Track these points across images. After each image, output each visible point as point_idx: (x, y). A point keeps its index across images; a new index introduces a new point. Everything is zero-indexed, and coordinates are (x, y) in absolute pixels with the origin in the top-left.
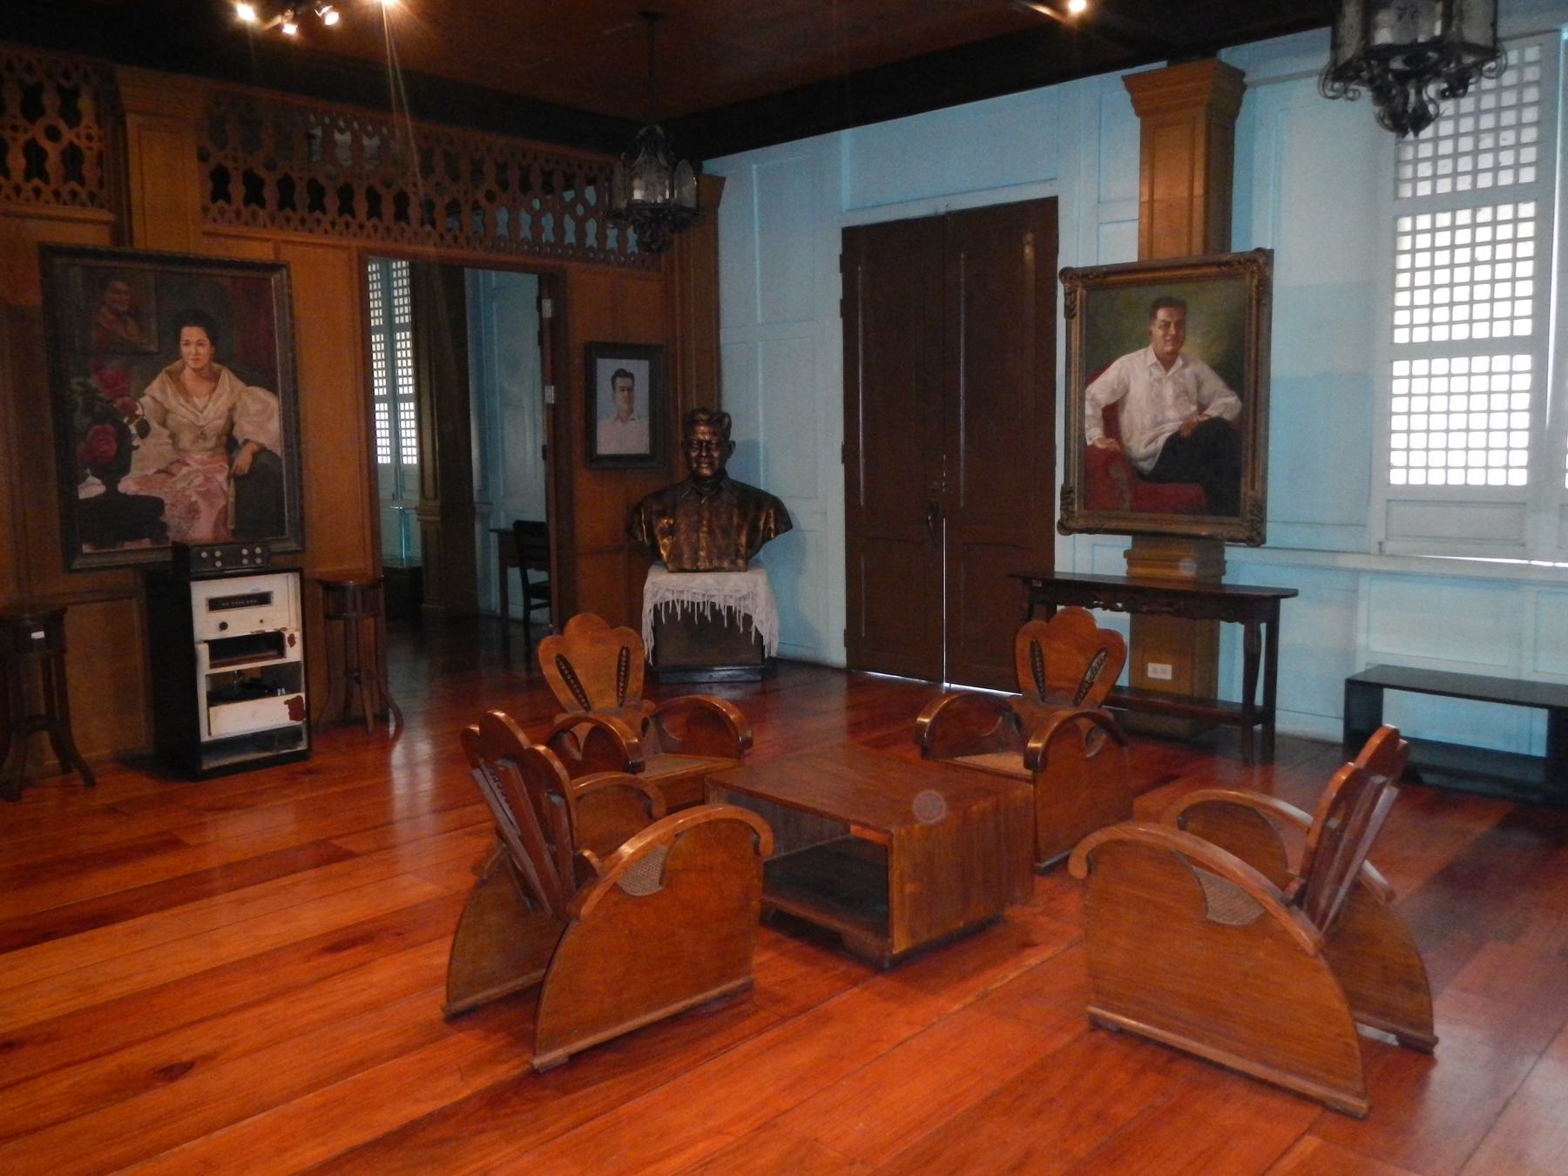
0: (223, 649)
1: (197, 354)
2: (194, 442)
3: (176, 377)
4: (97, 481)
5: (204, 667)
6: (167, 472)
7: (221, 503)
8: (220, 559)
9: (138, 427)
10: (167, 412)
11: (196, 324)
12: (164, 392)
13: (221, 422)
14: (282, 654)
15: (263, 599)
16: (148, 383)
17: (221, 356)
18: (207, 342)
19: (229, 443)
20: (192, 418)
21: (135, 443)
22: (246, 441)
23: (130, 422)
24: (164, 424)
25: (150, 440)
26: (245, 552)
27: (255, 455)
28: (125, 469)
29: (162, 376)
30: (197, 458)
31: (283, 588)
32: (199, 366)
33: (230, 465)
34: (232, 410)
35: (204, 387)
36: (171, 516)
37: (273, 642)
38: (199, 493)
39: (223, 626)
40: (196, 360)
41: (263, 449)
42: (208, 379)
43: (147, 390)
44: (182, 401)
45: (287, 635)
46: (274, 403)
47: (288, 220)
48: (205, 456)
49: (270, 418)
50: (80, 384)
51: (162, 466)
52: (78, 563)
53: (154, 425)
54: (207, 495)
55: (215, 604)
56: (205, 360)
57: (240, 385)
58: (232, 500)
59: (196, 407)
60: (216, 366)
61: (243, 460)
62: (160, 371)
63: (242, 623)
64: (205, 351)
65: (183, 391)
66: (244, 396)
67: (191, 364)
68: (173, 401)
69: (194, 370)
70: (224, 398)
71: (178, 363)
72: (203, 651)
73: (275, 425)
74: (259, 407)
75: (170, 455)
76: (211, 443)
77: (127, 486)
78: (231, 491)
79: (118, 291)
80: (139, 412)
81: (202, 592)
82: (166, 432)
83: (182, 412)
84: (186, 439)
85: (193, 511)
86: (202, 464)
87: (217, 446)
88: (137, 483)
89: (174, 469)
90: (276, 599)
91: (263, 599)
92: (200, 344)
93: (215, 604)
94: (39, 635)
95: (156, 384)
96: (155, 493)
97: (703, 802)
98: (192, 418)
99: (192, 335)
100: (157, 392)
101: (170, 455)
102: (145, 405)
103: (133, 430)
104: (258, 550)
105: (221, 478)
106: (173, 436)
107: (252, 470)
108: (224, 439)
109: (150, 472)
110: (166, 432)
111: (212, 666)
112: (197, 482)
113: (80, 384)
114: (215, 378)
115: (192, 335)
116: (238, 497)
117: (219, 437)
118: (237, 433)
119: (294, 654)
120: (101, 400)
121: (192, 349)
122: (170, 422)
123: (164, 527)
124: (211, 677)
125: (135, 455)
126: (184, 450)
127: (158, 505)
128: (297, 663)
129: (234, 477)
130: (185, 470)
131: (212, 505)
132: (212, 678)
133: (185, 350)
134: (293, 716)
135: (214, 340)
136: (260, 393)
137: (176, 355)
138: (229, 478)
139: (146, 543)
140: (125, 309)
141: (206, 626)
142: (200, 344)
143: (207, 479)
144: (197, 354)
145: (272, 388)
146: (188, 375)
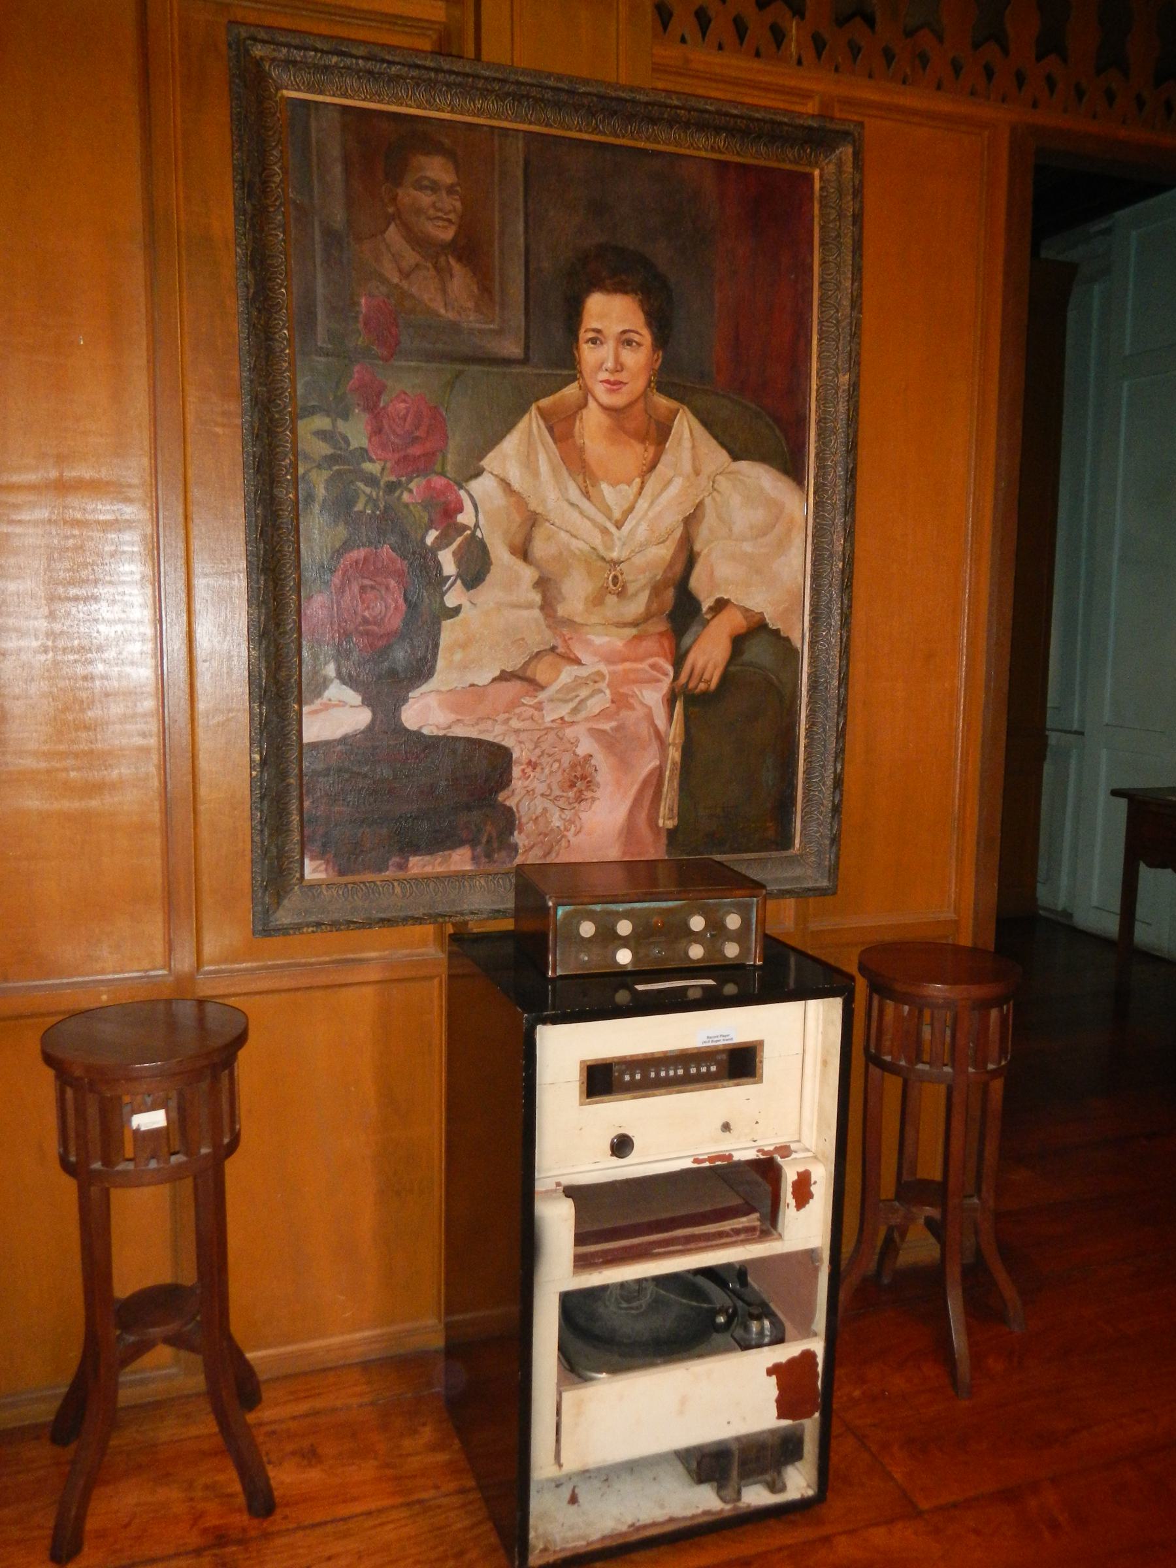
0: (618, 1214)
1: (619, 367)
2: (597, 600)
3: (561, 428)
4: (352, 696)
5: (558, 1272)
6: (520, 677)
7: (648, 763)
8: (633, 1076)
9: (460, 558)
10: (533, 520)
11: (620, 288)
12: (529, 463)
13: (664, 552)
14: (770, 1224)
15: (741, 1063)
16: (494, 440)
17: (674, 377)
18: (646, 337)
19: (681, 609)
20: (597, 540)
21: (450, 601)
22: (721, 605)
23: (443, 541)
24: (523, 552)
25: (489, 593)
26: (697, 923)
27: (738, 642)
28: (422, 670)
29: (531, 423)
30: (601, 642)
31: (800, 1038)
32: (618, 400)
33: (678, 662)
34: (691, 521)
35: (634, 454)
36: (526, 794)
37: (748, 1188)
38: (598, 735)
39: (622, 1146)
40: (614, 386)
41: (758, 628)
42: (642, 437)
43: (490, 462)
44: (574, 493)
45: (790, 1175)
46: (798, 507)
47: (855, 50)
48: (616, 640)
49: (782, 545)
50: (322, 435)
51: (513, 664)
52: (283, 917)
53: (500, 553)
54: (612, 742)
55: (601, 1080)
56: (637, 385)
57: (715, 456)
58: (674, 754)
59: (607, 512)
60: (663, 402)
61: (710, 653)
62: (524, 410)
63: (675, 1133)
64: (638, 360)
65: (576, 462)
66: (723, 483)
67: (600, 391)
68: (553, 493)
69: (606, 409)
70: (674, 490)
71: (571, 391)
72: (557, 1221)
73: (794, 563)
74: (759, 515)
75: (538, 635)
76: (636, 607)
77: (425, 712)
78: (675, 733)
79: (434, 187)
80: (466, 518)
81: (565, 1050)
82: (528, 574)
83: (573, 522)
84: (576, 593)
85: (580, 781)
86: (609, 659)
87: (648, 617)
88: (456, 707)
89: (541, 672)
90: (769, 1063)
91: (741, 1063)
92: (625, 340)
93: (601, 1080)
94: (152, 1120)
95: (511, 444)
96: (494, 734)
97: (555, 443)
98: (597, 540)
99: (610, 314)
100: (517, 466)
101: (538, 635)
102: (483, 501)
103: (448, 562)
104: (733, 922)
105: (653, 697)
106: (542, 584)
107: (725, 678)
108: (670, 594)
109: (484, 677)
110: (528, 574)
111: (582, 1262)
112: (597, 704)
113: (322, 435)
114: (658, 434)
115: (610, 314)
116: (688, 750)
117: (656, 590)
118: (698, 583)
119: (806, 1228)
120: (372, 481)
121: (606, 352)
122: (540, 548)
123: (508, 820)
124: (571, 1303)
125: (449, 632)
126: (569, 622)
127: (495, 763)
128: (810, 1255)
129: (693, 703)
130: (568, 674)
131: (624, 764)
132: (571, 1303)
133: (589, 355)
134: (785, 1408)
135: (661, 323)
136: (762, 477)
137: (565, 364)
138: (671, 701)
139: (460, 860)
140: (448, 235)
141: (573, 1142)
142: (625, 340)
143: (621, 701)
144: (619, 367)
145: (793, 470)
146: (592, 424)
